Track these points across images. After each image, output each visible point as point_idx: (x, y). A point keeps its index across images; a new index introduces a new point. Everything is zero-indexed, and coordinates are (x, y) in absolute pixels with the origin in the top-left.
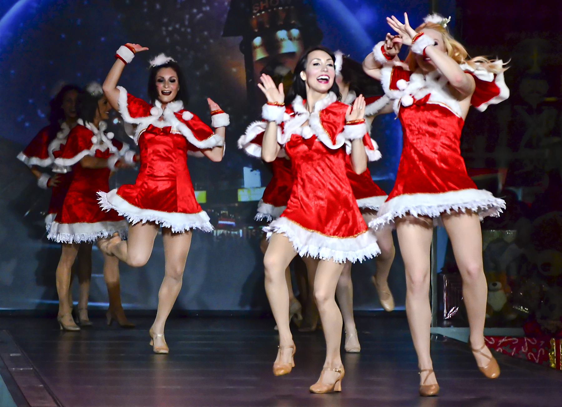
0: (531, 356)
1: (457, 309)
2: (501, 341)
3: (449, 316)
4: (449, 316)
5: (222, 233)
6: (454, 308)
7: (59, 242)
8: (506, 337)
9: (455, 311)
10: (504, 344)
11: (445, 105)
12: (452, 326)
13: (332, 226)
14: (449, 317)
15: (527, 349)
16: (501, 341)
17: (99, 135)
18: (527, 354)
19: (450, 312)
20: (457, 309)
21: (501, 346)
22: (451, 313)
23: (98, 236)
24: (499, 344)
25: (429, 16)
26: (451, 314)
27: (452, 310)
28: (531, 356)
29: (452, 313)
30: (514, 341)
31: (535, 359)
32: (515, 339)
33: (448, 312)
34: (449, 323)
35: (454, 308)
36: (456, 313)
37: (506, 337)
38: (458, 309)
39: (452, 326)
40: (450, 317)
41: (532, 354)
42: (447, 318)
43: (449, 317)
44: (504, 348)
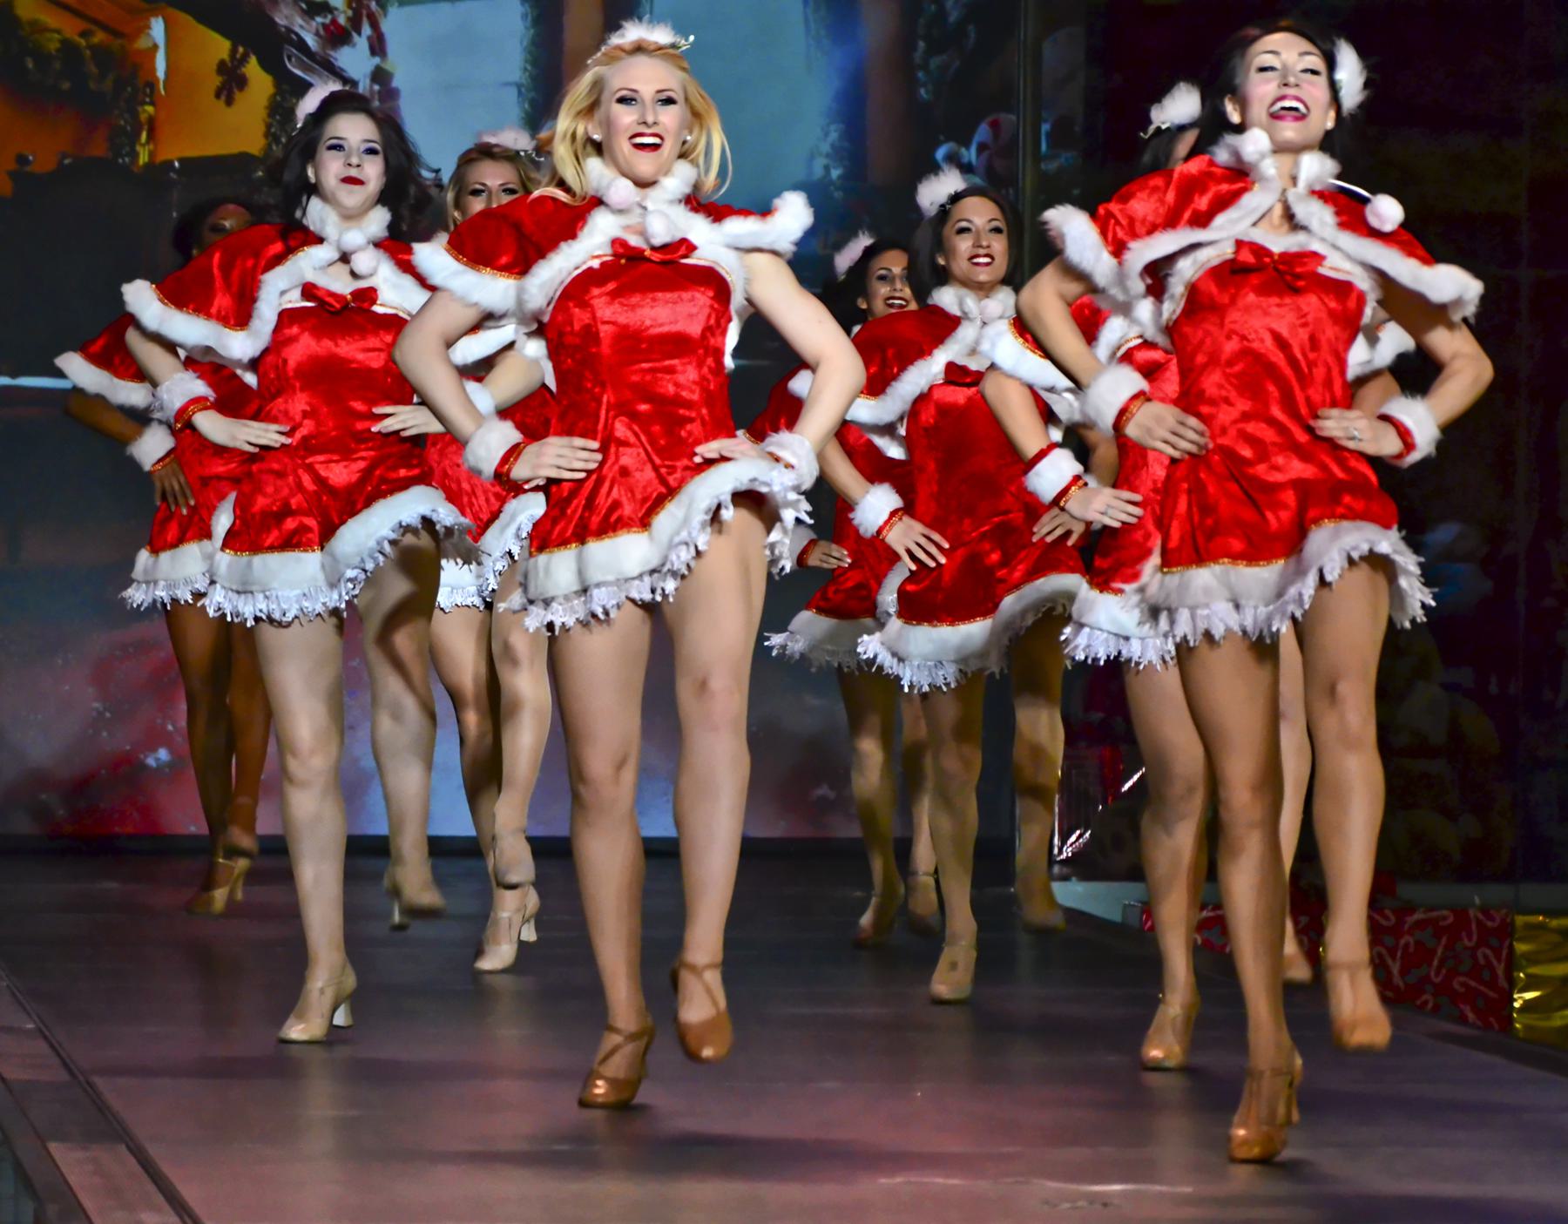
0: (1486, 957)
1: (1087, 835)
2: (1411, 920)
3: (1067, 852)
4: (1068, 853)
5: (1226, 630)
6: (1078, 832)
7: (1083, 658)
8: (1210, 907)
9: (1081, 840)
10: (1420, 925)
11: (577, 268)
12: (1074, 879)
13: (1125, 610)
14: (1065, 854)
15: (1475, 937)
16: (1411, 920)
17: (393, 334)
18: (1474, 949)
19: (1069, 842)
20: (1087, 835)
21: (1410, 932)
22: (1071, 845)
23: (550, 626)
24: (1406, 927)
25: (666, 26)
26: (1070, 849)
27: (1073, 838)
28: (1486, 957)
29: (1074, 846)
30: (1445, 918)
31: (1495, 962)
32: (1445, 912)
33: (1064, 841)
34: (1065, 870)
35: (1078, 832)
36: (1085, 844)
37: (1210, 907)
38: (1090, 835)
39: (1074, 879)
40: (1070, 855)
41: (1488, 952)
42: (1062, 857)
43: (1065, 854)
44: (1206, 934)
